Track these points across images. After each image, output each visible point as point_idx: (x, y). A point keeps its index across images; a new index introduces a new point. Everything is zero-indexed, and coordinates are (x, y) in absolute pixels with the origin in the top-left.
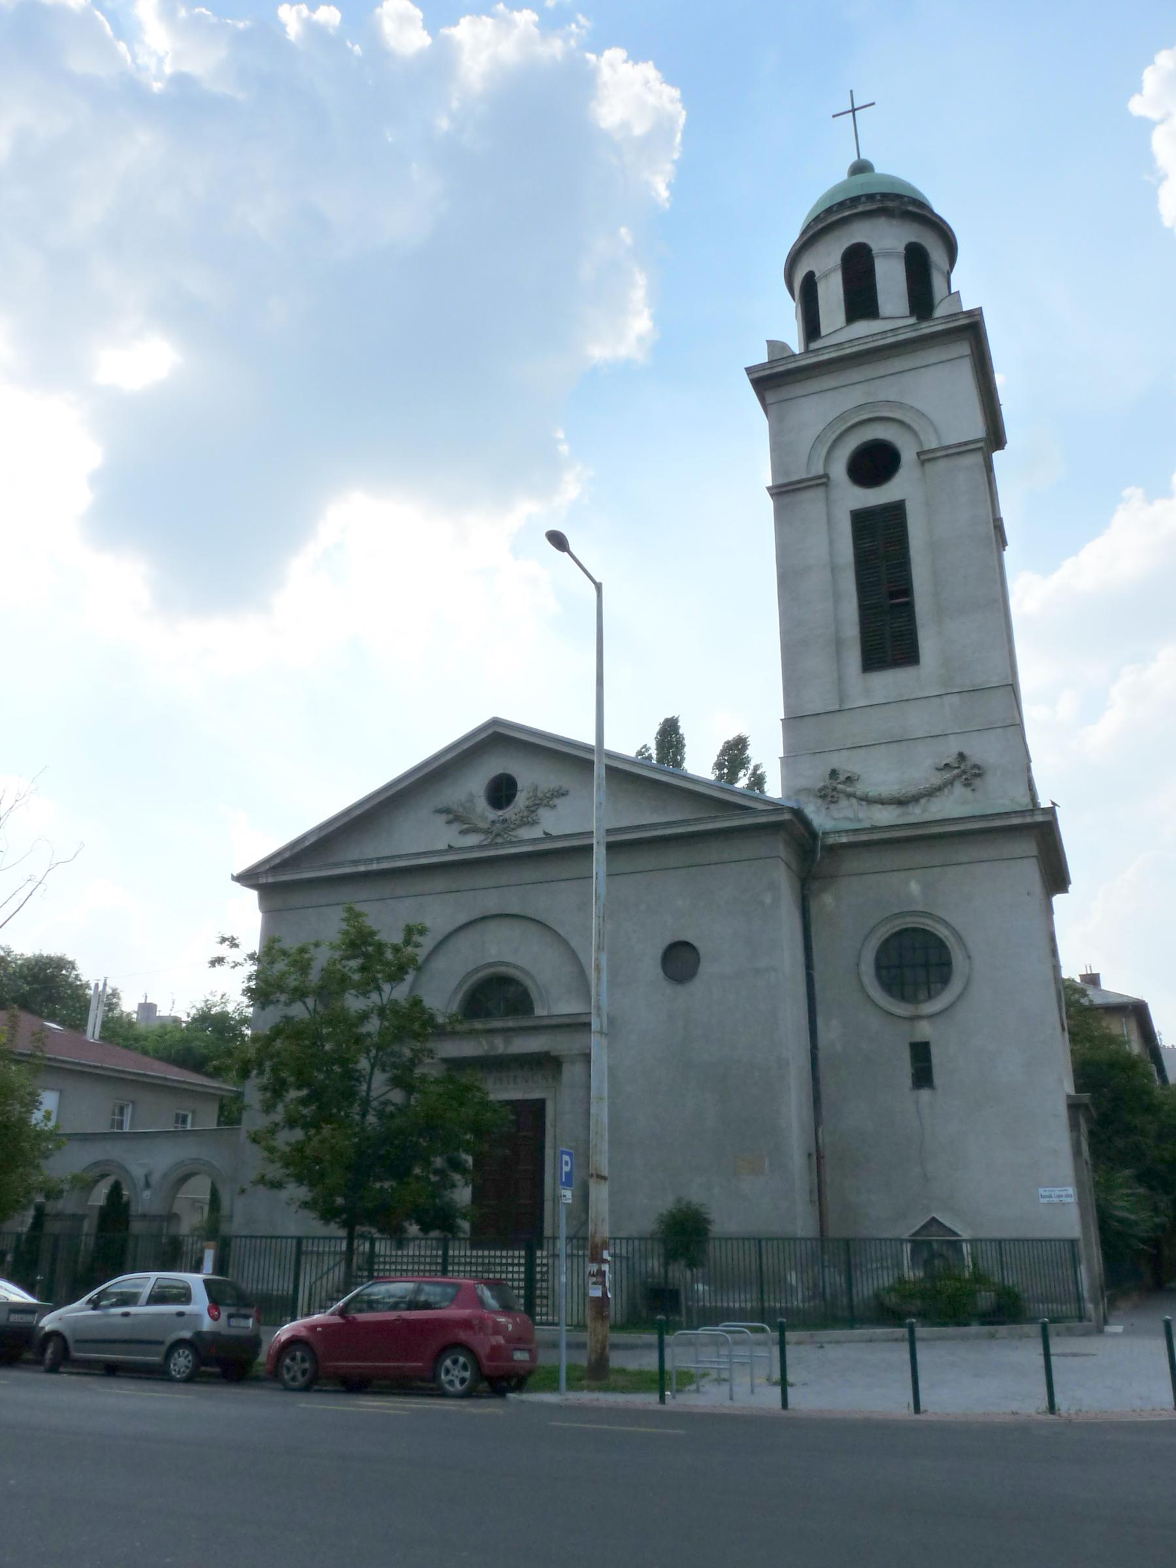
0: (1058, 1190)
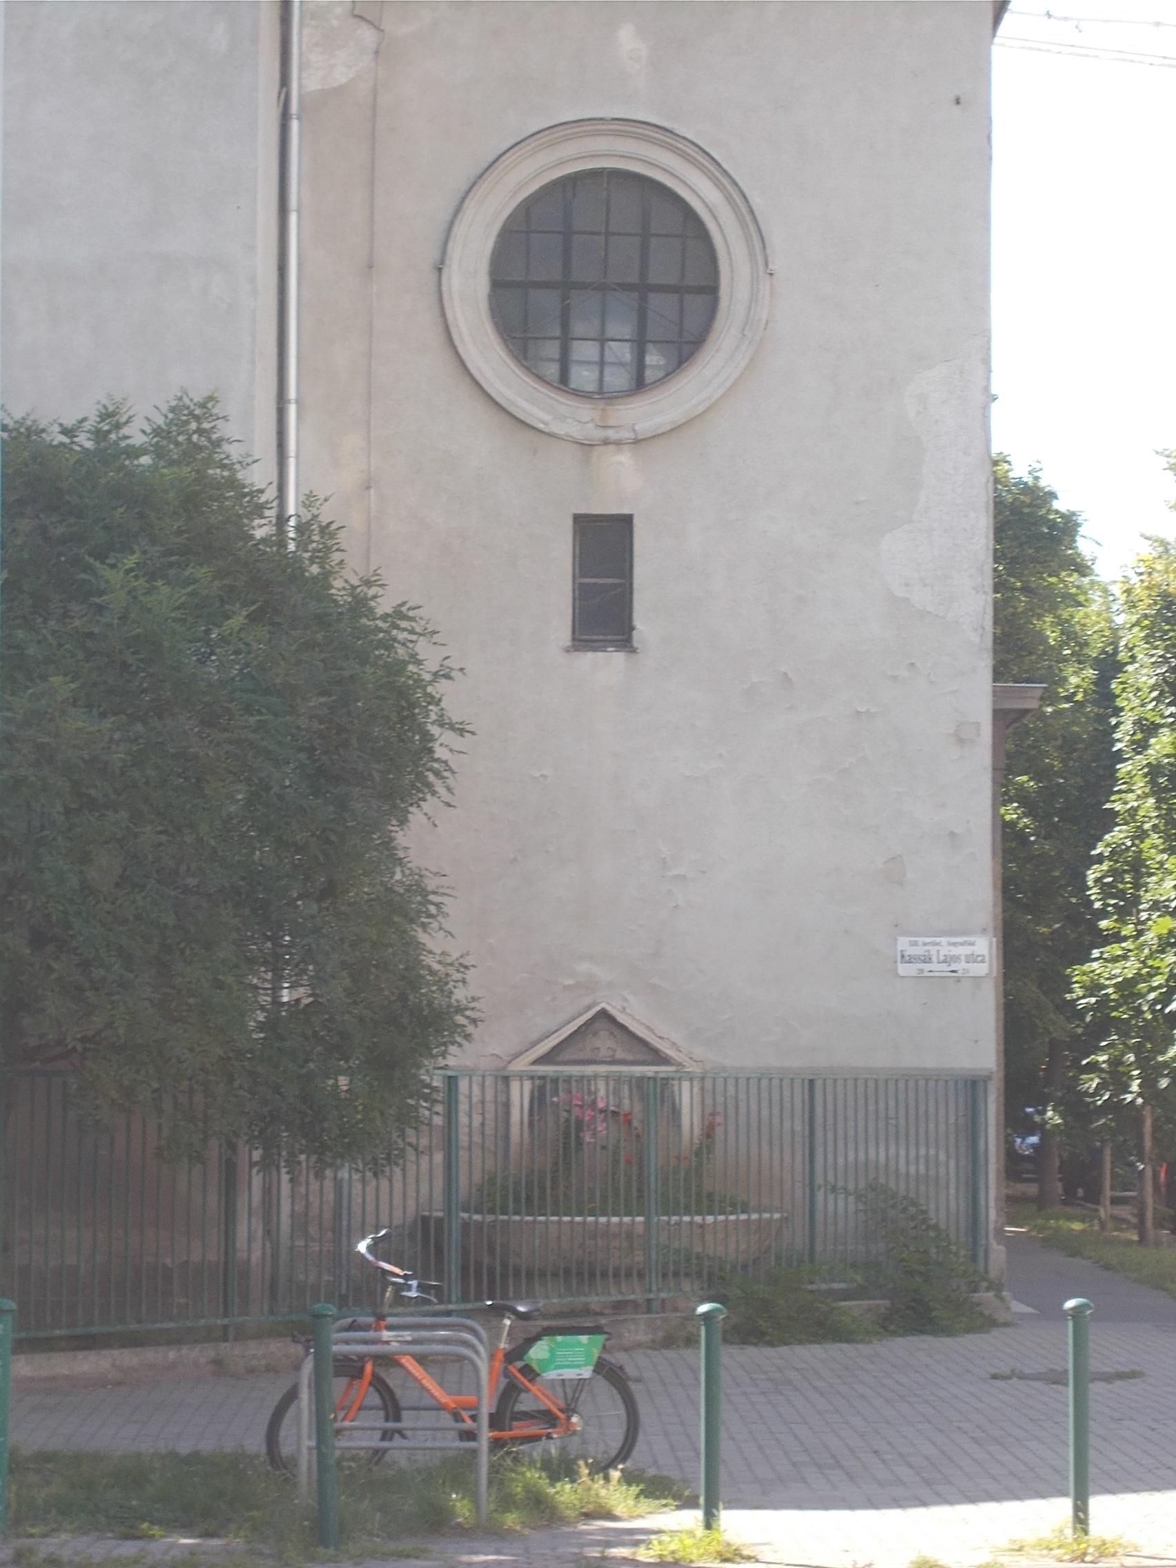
0: (951, 944)
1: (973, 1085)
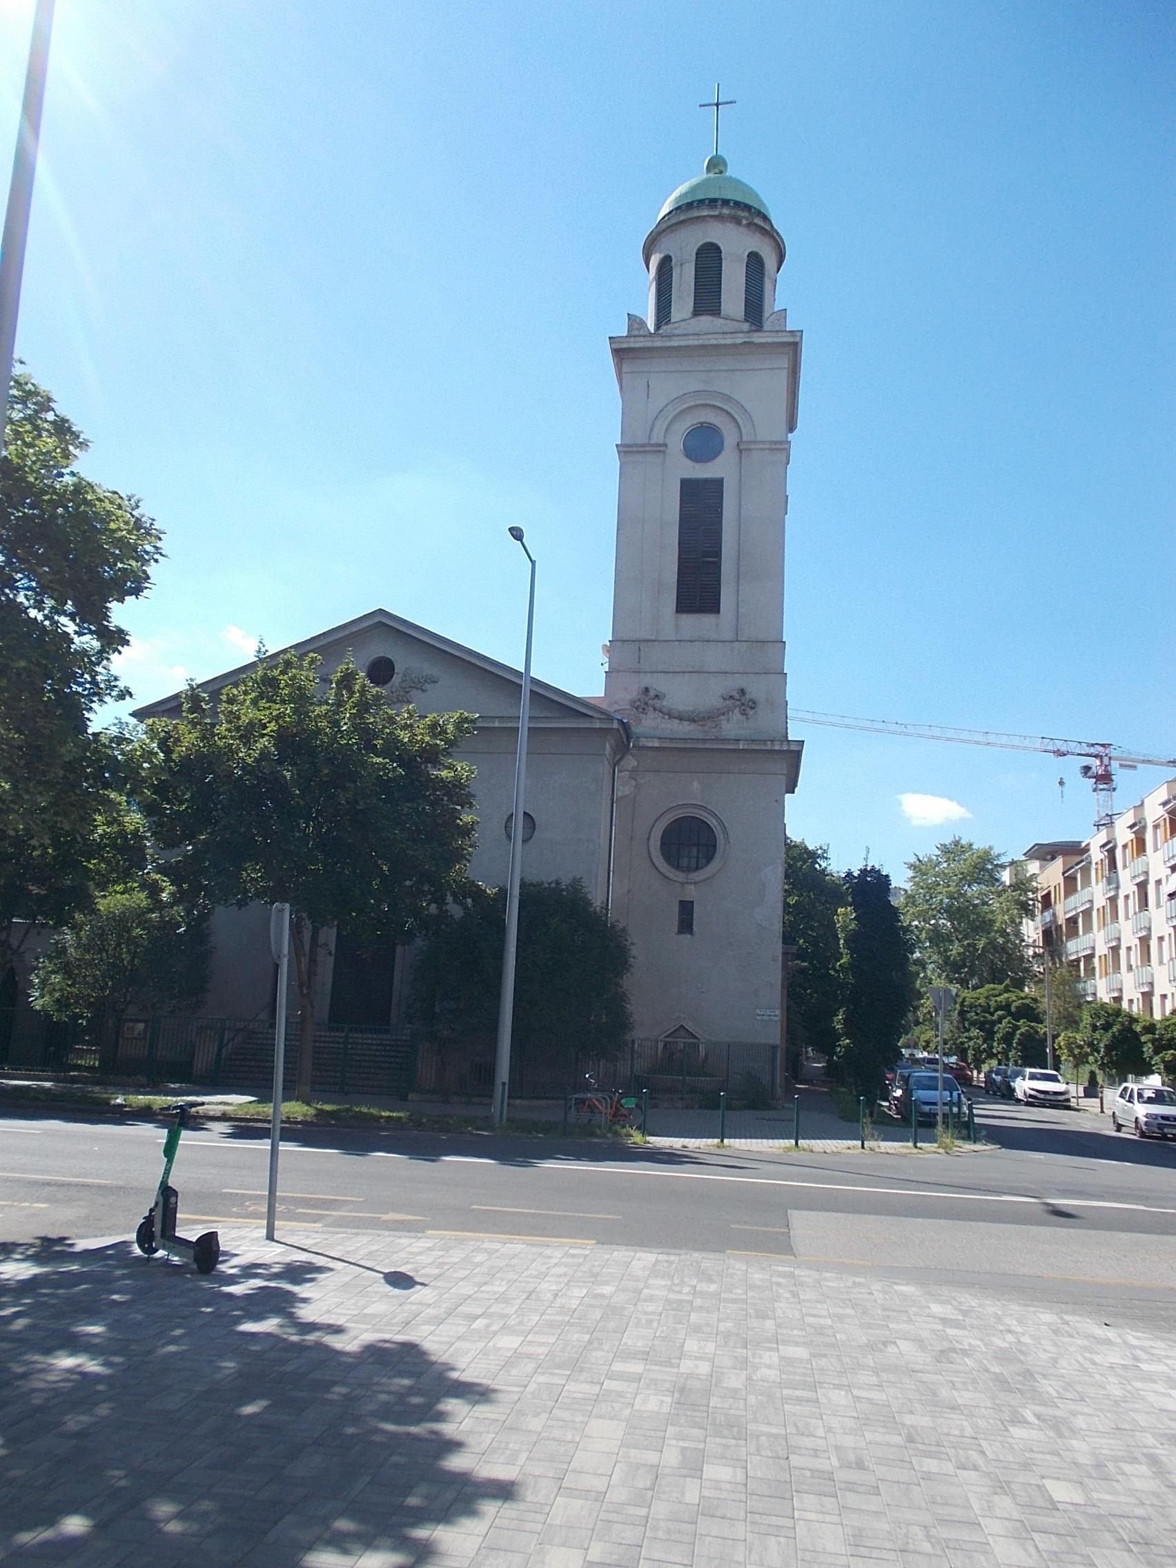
1: (774, 1048)
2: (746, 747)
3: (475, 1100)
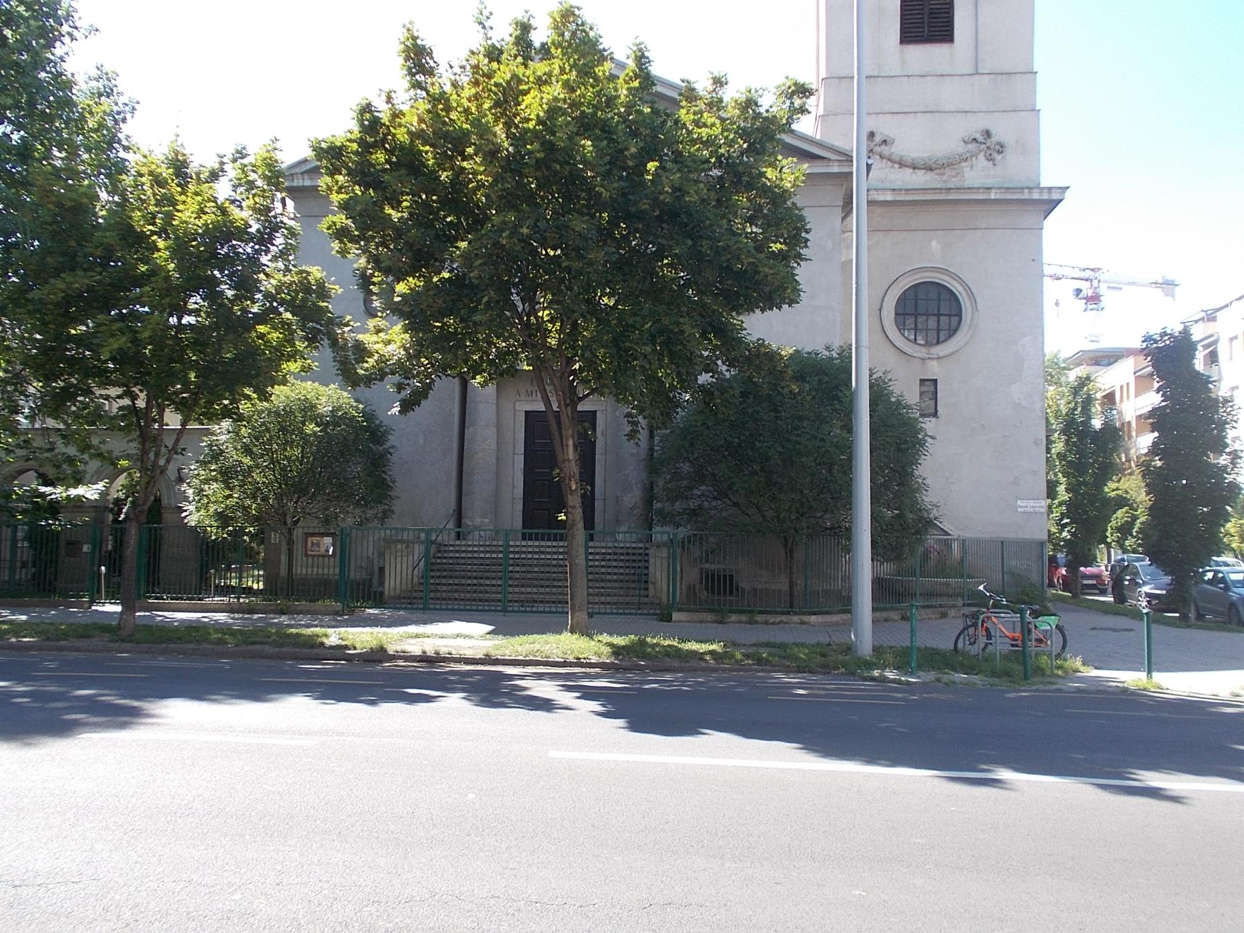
2: (998, 197)
3: (759, 618)
